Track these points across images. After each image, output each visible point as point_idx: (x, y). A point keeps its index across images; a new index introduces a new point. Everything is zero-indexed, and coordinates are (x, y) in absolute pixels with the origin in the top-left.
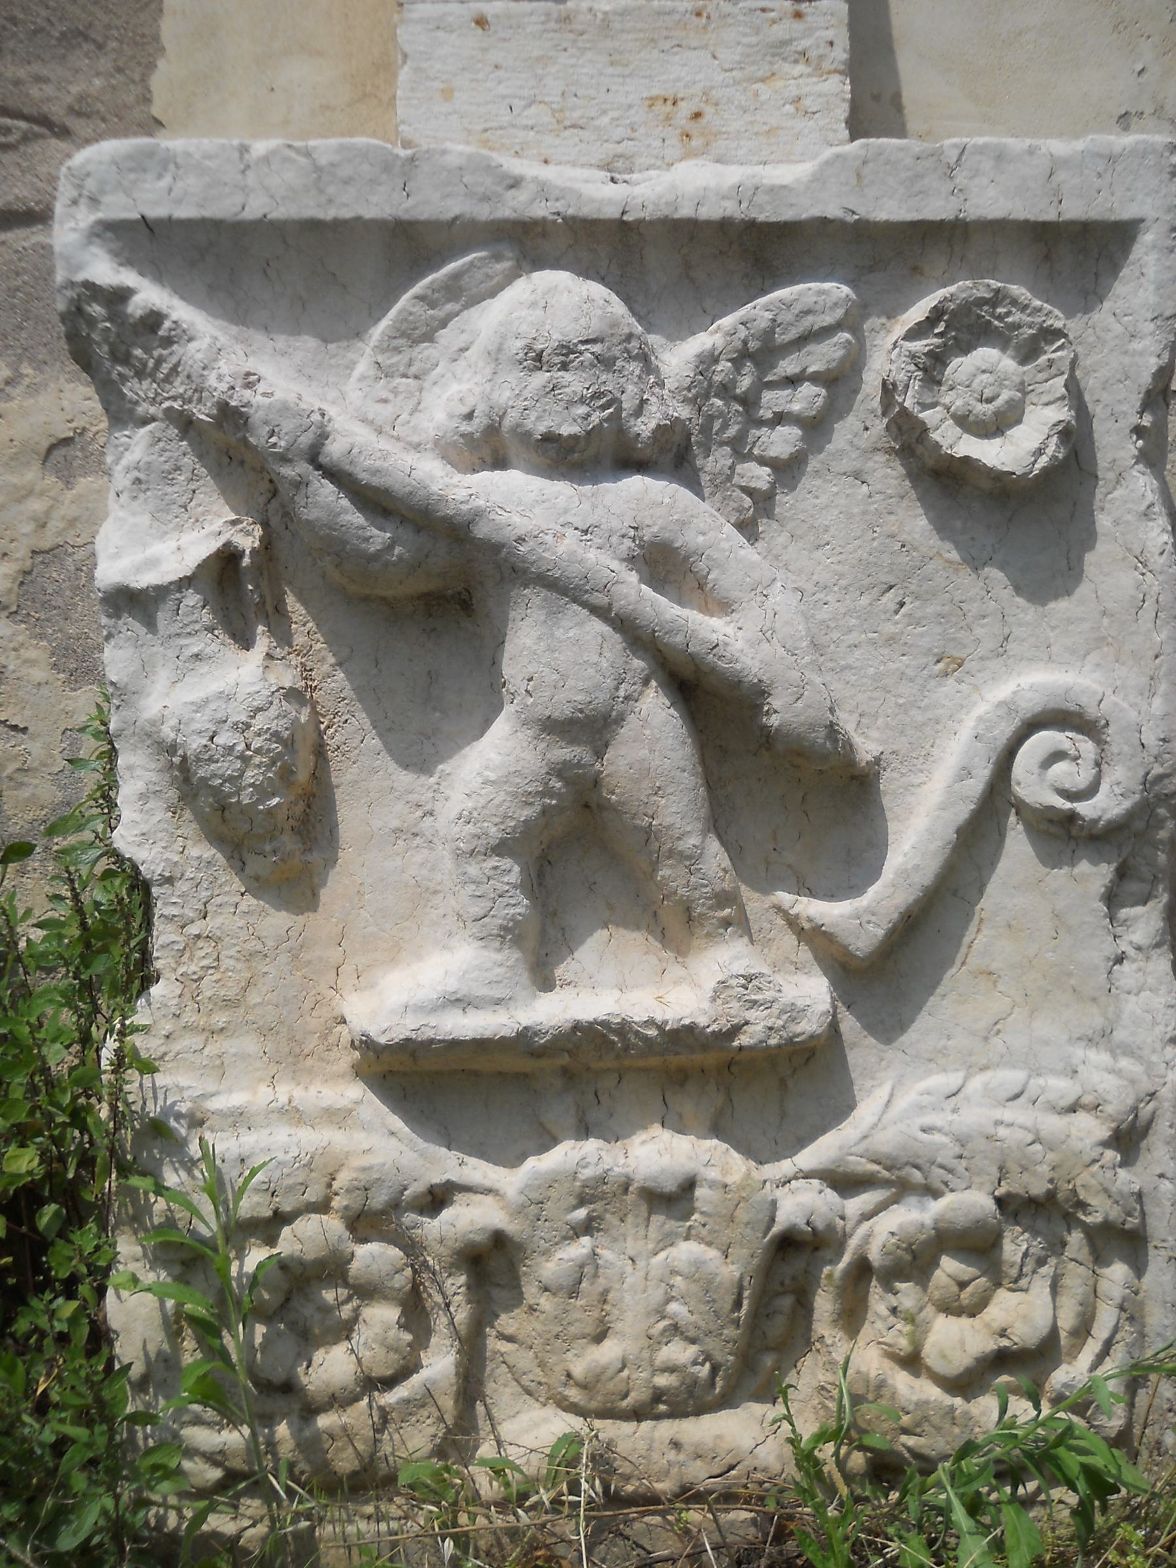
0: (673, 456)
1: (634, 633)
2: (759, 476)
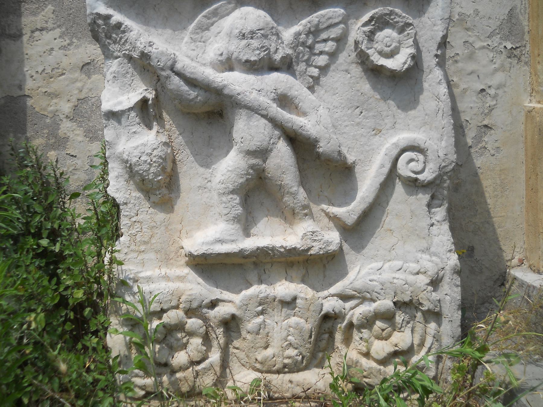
0: (287, 66)
1: (275, 123)
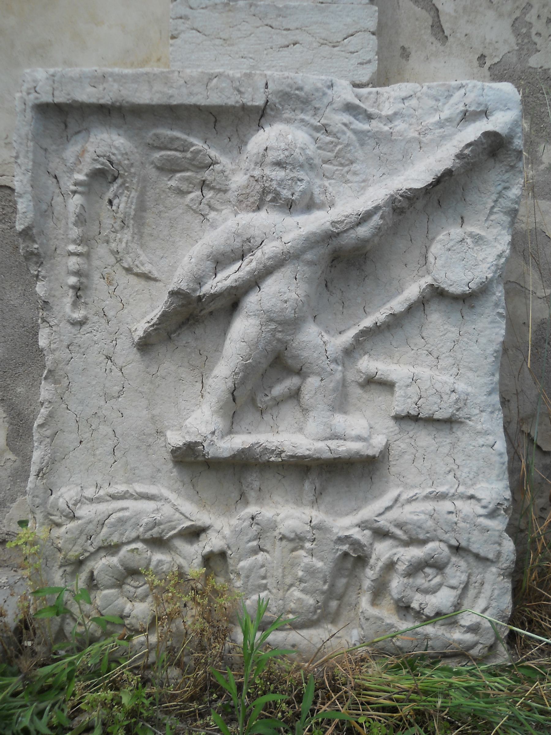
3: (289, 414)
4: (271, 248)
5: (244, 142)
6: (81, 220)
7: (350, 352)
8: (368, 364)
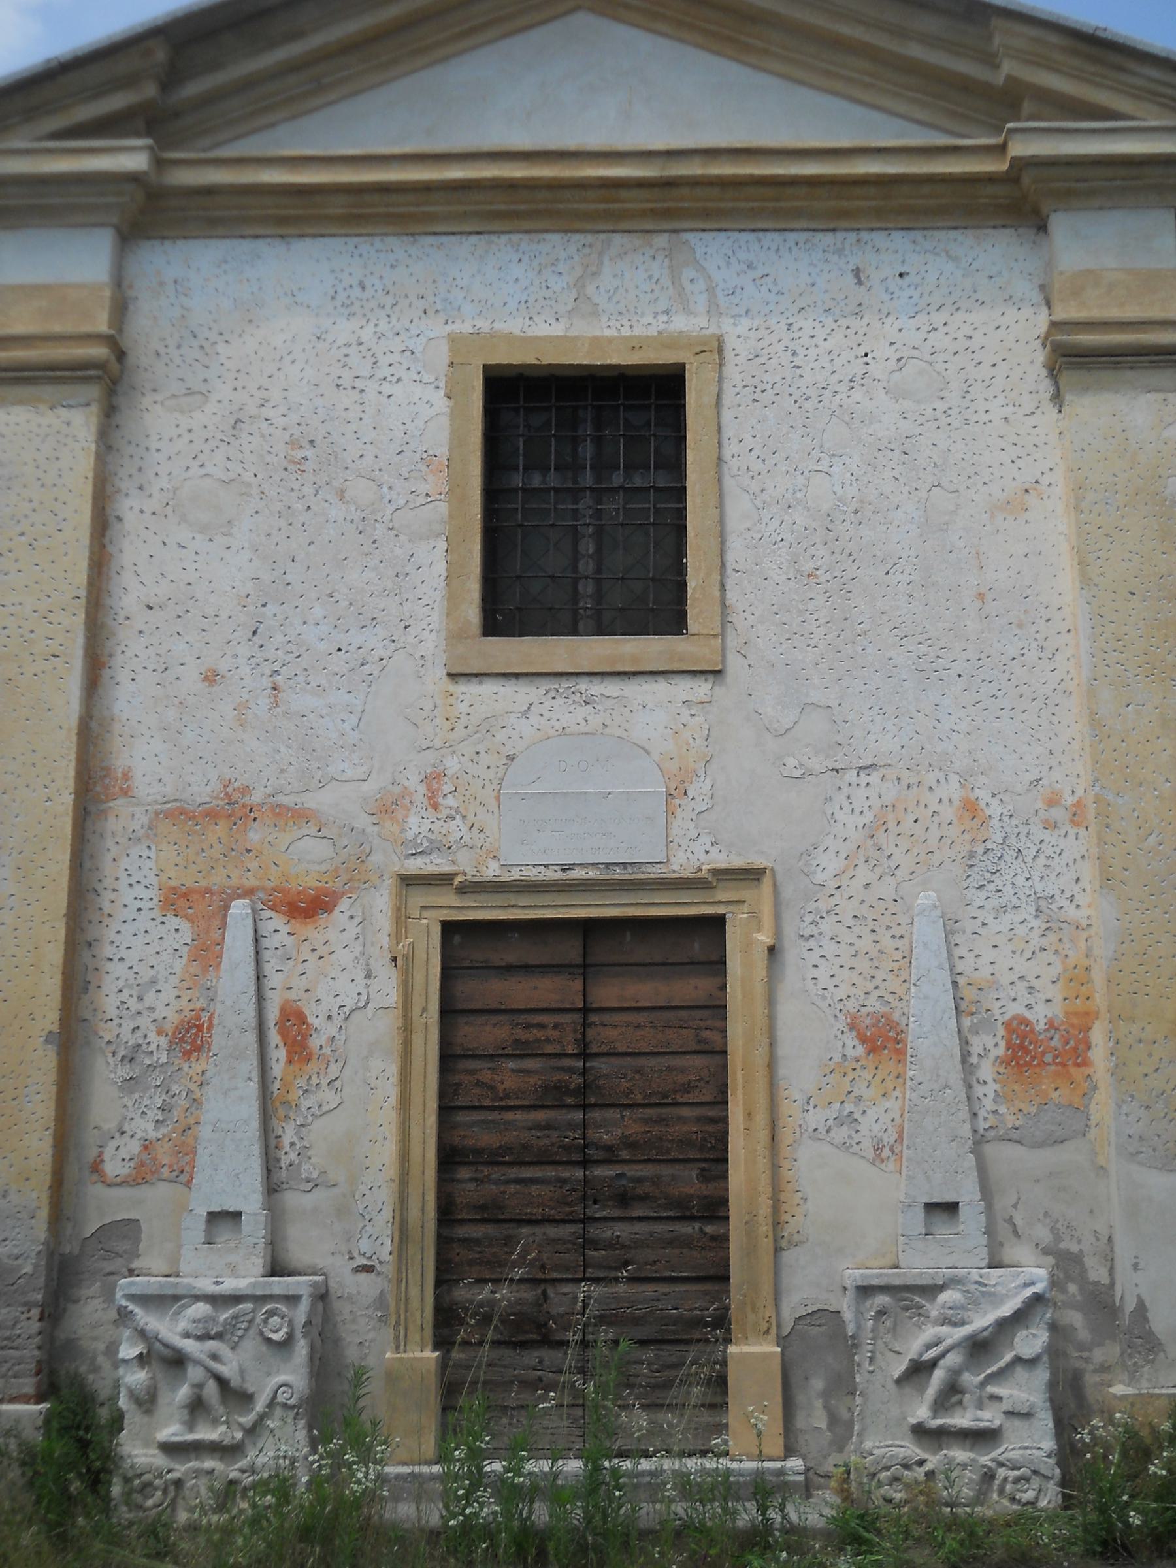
0: (219, 1336)
1: (208, 1370)
2: (236, 1339)
3: (958, 1411)
4: (949, 1342)
5: (935, 1298)
6: (872, 1331)
7: (983, 1384)
8: (991, 1389)
